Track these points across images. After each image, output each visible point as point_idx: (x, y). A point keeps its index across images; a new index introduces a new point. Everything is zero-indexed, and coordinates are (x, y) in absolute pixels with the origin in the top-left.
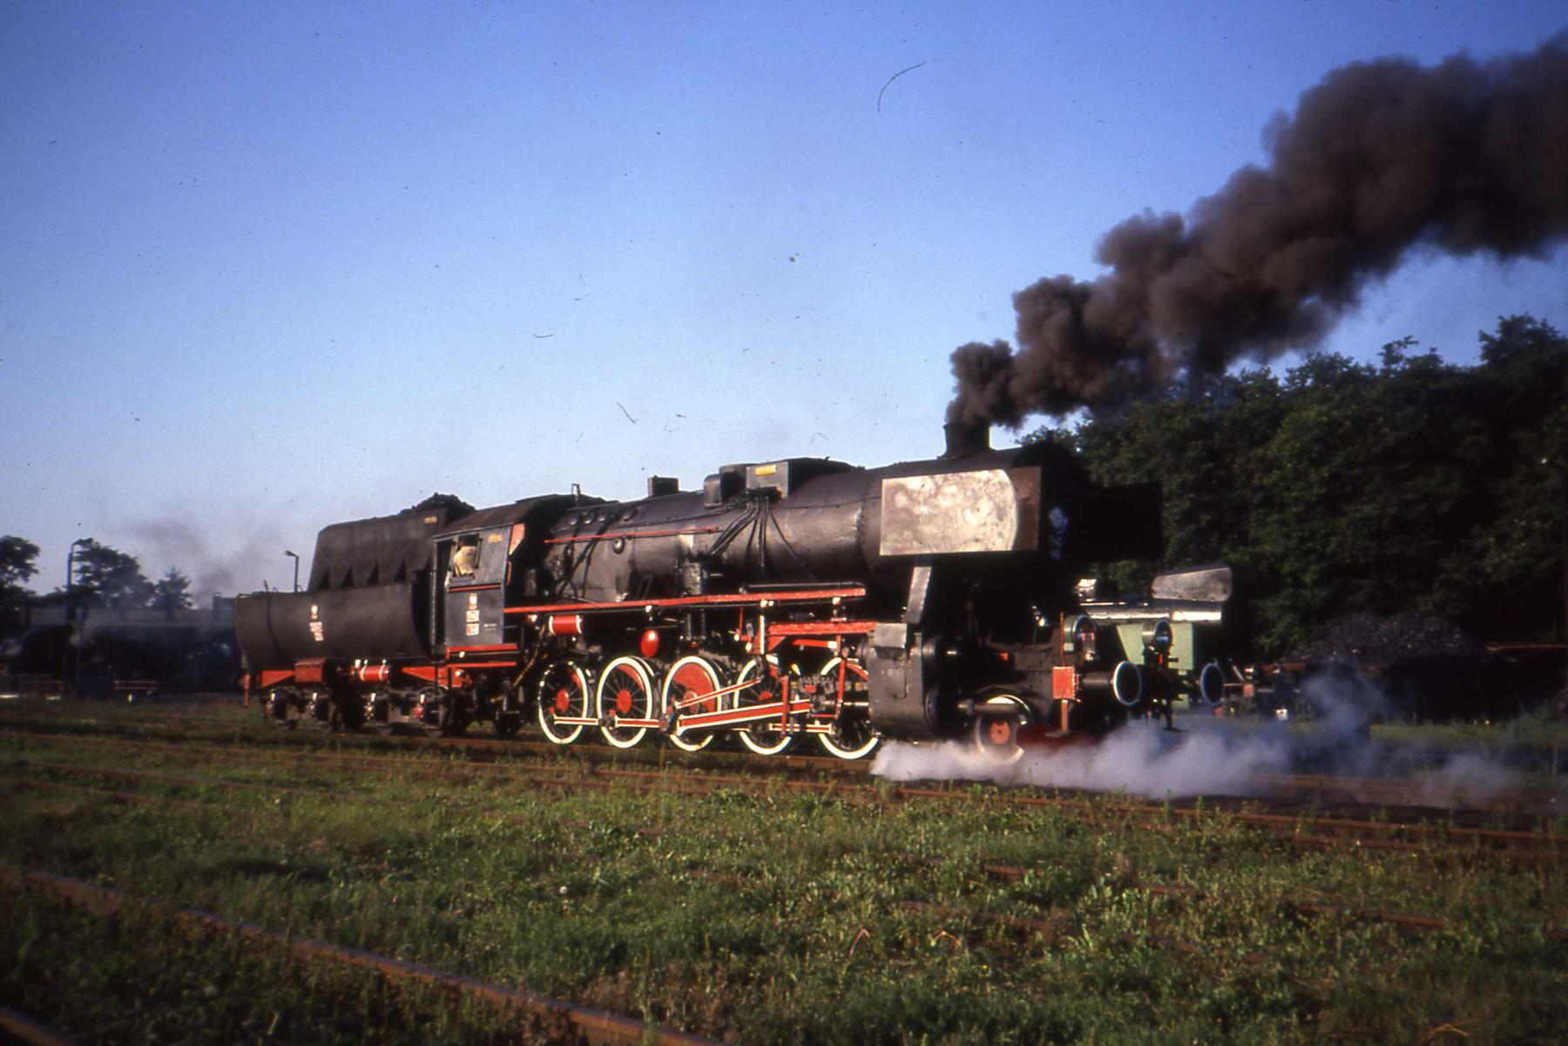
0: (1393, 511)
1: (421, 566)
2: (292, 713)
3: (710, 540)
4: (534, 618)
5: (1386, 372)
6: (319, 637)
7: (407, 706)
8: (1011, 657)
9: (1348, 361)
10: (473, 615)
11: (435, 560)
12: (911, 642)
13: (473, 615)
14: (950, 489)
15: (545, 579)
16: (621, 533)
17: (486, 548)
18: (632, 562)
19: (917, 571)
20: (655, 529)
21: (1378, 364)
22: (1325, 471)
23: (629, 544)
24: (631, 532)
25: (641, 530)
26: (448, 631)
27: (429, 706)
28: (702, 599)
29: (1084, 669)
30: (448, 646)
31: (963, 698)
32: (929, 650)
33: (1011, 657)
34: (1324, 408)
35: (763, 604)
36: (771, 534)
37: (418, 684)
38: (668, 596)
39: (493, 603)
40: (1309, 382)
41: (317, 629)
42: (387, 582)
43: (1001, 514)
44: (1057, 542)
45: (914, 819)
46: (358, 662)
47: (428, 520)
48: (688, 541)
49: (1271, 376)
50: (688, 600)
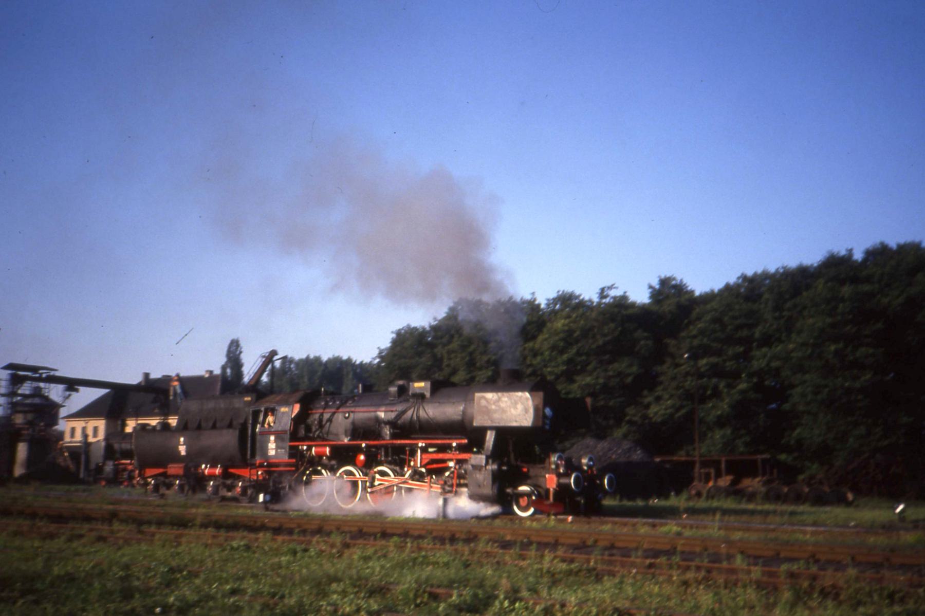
0: (601, 381)
1: (242, 421)
2: (163, 490)
3: (392, 416)
4: (305, 448)
5: (599, 304)
6: (183, 453)
7: (230, 488)
8: (528, 471)
9: (579, 296)
10: (272, 446)
11: (251, 418)
12: (487, 463)
13: (272, 446)
14: (505, 399)
15: (308, 429)
16: (348, 410)
17: (279, 415)
18: (353, 423)
19: (489, 433)
20: (365, 409)
21: (596, 299)
22: (565, 357)
23: (352, 415)
24: (353, 409)
25: (358, 409)
26: (258, 452)
27: (244, 489)
28: (391, 442)
29: (559, 475)
30: (258, 460)
31: (508, 487)
32: (495, 467)
33: (528, 471)
34: (567, 321)
35: (420, 445)
36: (422, 413)
37: (239, 478)
38: (374, 440)
39: (283, 440)
40: (558, 306)
41: (183, 450)
42: (222, 428)
43: (526, 411)
44: (548, 422)
45: (366, 559)
46: (203, 466)
47: (246, 399)
48: (382, 415)
49: (537, 302)
50: (383, 442)
